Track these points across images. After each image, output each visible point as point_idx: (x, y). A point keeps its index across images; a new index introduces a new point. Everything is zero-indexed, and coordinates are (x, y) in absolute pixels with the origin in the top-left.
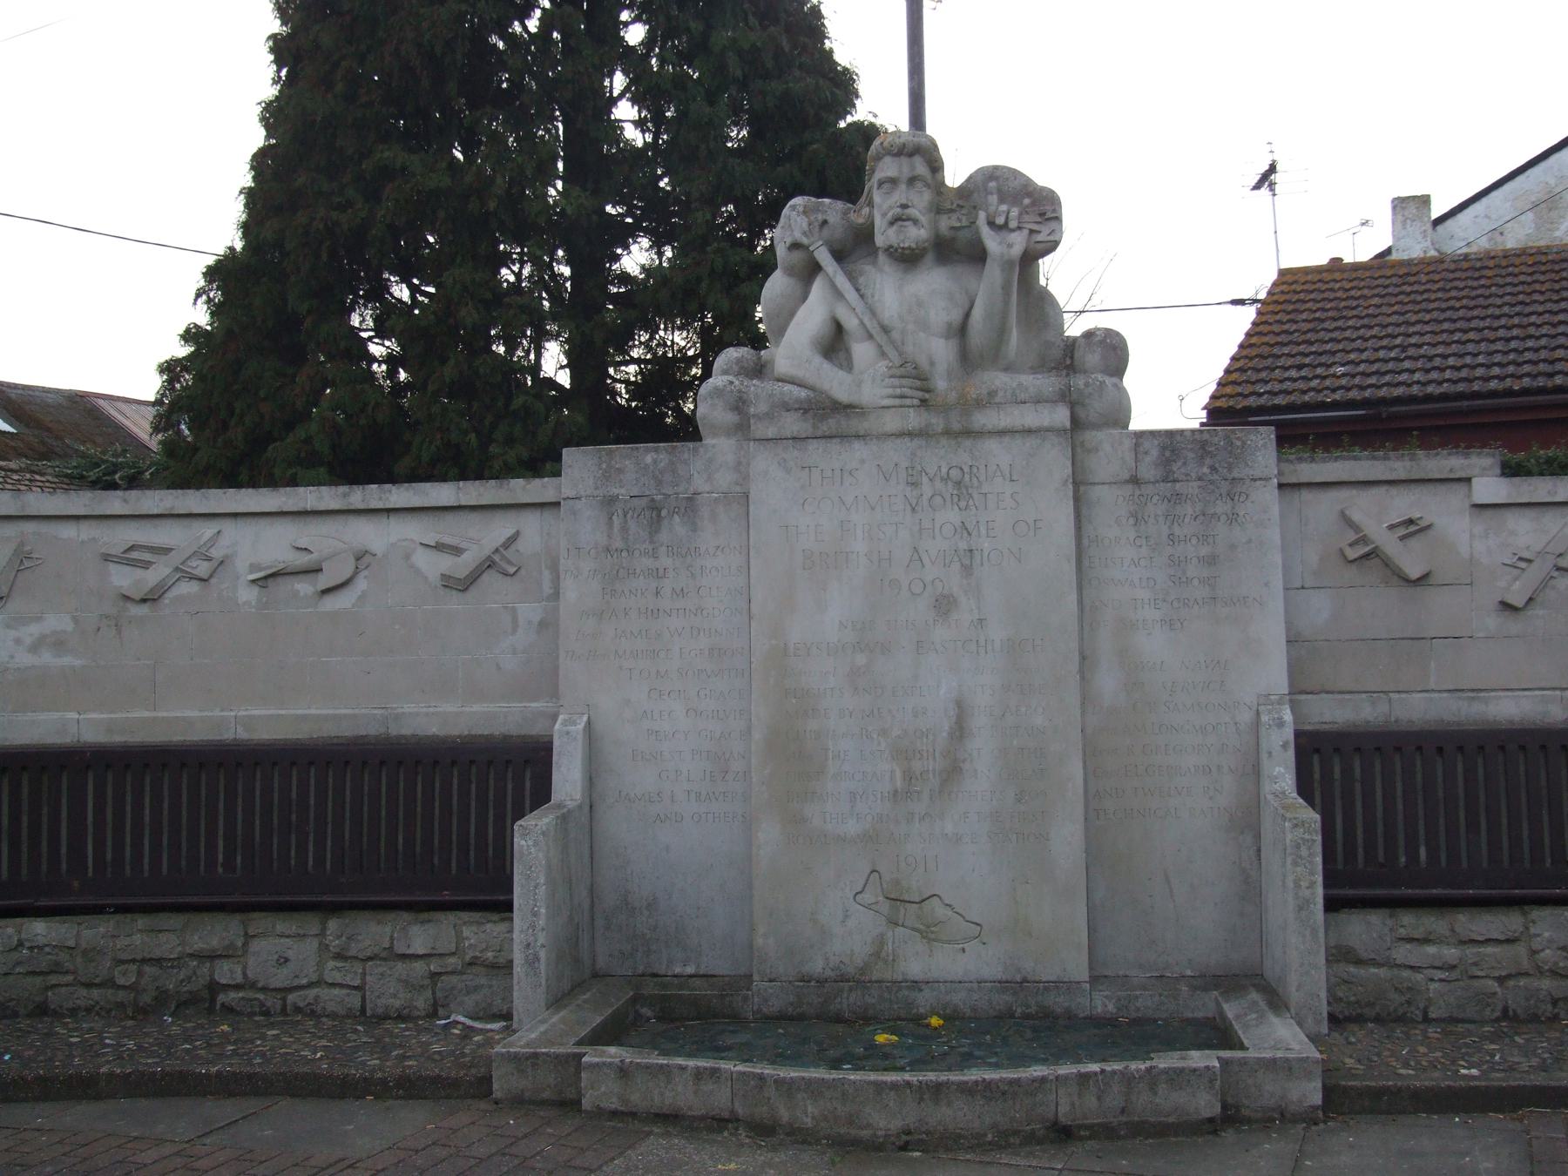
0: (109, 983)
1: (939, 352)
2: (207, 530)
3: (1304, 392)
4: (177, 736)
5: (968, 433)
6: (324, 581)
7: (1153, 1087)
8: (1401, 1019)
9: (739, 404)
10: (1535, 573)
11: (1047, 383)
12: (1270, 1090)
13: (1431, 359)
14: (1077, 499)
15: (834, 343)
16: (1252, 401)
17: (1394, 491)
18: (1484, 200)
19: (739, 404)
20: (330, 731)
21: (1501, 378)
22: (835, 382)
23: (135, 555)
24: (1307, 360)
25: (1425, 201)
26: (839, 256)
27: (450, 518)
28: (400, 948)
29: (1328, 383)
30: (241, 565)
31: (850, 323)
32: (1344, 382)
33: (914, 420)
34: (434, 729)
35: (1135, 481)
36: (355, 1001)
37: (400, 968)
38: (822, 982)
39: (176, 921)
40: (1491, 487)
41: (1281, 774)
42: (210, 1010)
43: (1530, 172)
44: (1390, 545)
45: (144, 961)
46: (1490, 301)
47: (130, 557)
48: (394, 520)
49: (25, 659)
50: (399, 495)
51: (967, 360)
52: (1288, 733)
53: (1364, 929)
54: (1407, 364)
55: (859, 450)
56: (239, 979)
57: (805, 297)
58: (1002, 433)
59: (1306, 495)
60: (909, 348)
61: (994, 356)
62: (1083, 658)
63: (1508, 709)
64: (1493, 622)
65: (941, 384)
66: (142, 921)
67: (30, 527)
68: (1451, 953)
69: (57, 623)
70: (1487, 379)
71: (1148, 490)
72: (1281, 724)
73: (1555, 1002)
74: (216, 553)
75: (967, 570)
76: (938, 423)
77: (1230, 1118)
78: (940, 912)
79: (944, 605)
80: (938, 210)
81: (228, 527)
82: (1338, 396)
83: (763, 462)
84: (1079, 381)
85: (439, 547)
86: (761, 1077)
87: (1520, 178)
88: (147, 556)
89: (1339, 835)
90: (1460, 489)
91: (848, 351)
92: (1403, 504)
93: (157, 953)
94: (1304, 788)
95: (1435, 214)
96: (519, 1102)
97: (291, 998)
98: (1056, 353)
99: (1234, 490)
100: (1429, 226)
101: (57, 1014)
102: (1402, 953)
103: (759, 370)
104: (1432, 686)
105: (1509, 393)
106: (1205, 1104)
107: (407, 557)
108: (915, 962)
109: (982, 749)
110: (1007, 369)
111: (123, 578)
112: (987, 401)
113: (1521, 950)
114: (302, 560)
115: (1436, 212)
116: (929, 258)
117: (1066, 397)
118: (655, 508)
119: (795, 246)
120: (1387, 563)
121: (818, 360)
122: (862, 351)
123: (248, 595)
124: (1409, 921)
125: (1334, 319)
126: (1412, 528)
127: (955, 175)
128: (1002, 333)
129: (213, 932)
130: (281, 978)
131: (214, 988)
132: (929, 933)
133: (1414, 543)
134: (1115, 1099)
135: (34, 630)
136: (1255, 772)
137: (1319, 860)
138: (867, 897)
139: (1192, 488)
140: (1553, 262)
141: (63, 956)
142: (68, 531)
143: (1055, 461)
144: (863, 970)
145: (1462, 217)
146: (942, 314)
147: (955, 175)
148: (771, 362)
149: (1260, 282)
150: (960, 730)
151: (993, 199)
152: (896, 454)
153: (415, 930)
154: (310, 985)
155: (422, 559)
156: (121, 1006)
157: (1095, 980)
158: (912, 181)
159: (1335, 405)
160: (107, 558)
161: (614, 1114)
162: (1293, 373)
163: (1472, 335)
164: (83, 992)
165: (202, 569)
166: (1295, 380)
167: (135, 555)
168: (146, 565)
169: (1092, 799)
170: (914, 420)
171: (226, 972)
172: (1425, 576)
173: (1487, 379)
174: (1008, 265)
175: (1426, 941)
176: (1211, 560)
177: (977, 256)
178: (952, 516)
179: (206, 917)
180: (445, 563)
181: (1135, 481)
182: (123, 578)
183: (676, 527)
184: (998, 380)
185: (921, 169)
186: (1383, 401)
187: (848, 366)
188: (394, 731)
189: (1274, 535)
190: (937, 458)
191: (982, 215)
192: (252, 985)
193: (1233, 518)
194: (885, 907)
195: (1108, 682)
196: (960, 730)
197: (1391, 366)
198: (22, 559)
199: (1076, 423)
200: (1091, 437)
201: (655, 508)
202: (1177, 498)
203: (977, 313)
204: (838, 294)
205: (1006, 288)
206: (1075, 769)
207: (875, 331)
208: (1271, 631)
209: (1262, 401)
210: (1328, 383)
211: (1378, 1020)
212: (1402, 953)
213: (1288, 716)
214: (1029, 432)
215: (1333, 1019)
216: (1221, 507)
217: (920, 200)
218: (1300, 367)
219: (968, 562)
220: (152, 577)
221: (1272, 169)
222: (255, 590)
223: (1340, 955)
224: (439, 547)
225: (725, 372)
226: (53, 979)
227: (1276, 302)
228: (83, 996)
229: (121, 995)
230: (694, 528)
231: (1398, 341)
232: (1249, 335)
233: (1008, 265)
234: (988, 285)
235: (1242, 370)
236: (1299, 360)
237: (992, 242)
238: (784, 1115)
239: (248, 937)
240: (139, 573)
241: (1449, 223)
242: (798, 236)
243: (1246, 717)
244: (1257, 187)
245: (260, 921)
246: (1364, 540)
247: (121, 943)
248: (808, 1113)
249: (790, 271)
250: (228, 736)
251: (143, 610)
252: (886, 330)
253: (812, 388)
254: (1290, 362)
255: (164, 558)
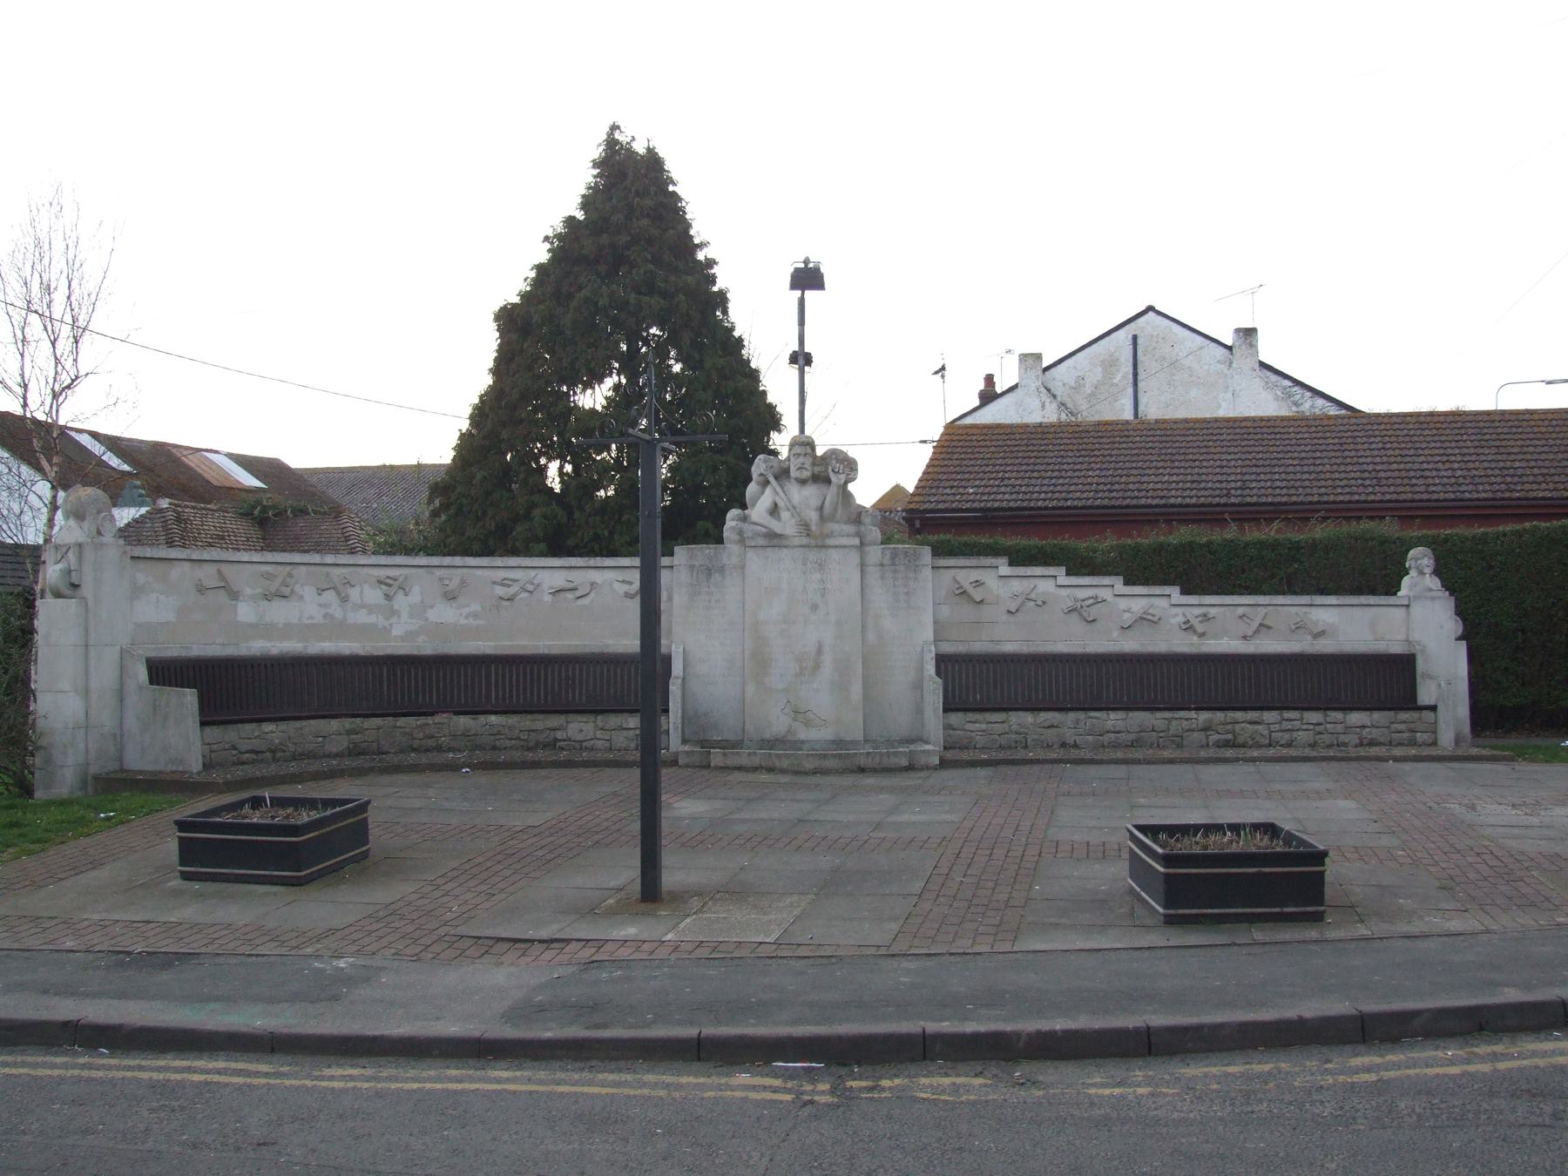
0: (518, 738)
1: (813, 516)
2: (532, 573)
3: (953, 502)
4: (521, 652)
5: (824, 547)
6: (578, 593)
7: (888, 757)
8: (967, 748)
9: (741, 533)
10: (1019, 600)
11: (851, 529)
12: (923, 760)
13: (1014, 487)
14: (862, 571)
15: (774, 511)
16: (927, 506)
17: (972, 570)
18: (1074, 358)
19: (741, 533)
20: (580, 650)
21: (1044, 500)
22: (776, 526)
23: (505, 582)
24: (956, 484)
25: (1038, 357)
26: (776, 478)
27: (627, 570)
28: (625, 726)
29: (964, 498)
30: (545, 587)
31: (781, 504)
32: (972, 497)
33: (805, 541)
34: (621, 650)
35: (882, 565)
36: (608, 745)
37: (625, 733)
38: (769, 741)
39: (541, 716)
40: (1005, 570)
41: (930, 669)
42: (554, 748)
43: (1101, 342)
44: (970, 589)
45: (530, 731)
46: (1047, 454)
47: (504, 583)
48: (606, 570)
49: (463, 622)
50: (609, 562)
51: (823, 519)
52: (933, 655)
53: (956, 718)
54: (1002, 489)
55: (785, 551)
56: (565, 737)
57: (763, 493)
58: (836, 547)
59: (942, 571)
60: (803, 515)
61: (832, 518)
62: (863, 627)
63: (1009, 648)
64: (1004, 617)
65: (814, 528)
66: (529, 716)
67: (465, 570)
68: (984, 726)
69: (475, 607)
70: (1038, 500)
71: (886, 568)
72: (930, 651)
73: (1016, 742)
74: (535, 582)
75: (823, 595)
76: (813, 542)
77: (910, 768)
78: (811, 716)
79: (815, 607)
80: (814, 464)
81: (541, 571)
82: (968, 505)
83: (751, 554)
84: (863, 528)
85: (623, 582)
86: (770, 754)
87: (1094, 346)
88: (510, 583)
89: (957, 693)
90: (995, 570)
91: (779, 513)
92: (975, 575)
93: (535, 728)
94: (938, 673)
95: (1044, 366)
96: (687, 766)
97: (585, 744)
98: (854, 516)
99: (917, 569)
100: (1040, 372)
101: (499, 749)
102: (969, 726)
103: (744, 519)
104: (984, 638)
105: (1046, 508)
106: (904, 762)
107: (611, 585)
108: (803, 734)
109: (827, 659)
110: (837, 522)
111: (500, 591)
112: (831, 535)
113: (1006, 725)
114: (570, 585)
115: (1046, 363)
116: (810, 481)
117: (858, 534)
118: (709, 570)
119: (761, 475)
120: (969, 596)
121: (769, 517)
122: (785, 515)
123: (548, 598)
124: (971, 716)
125: (971, 459)
126: (978, 584)
127: (820, 452)
128: (836, 509)
129: (555, 721)
130: (580, 737)
131: (556, 740)
132: (807, 724)
133: (978, 589)
134: (877, 759)
135: (466, 611)
136: (921, 668)
137: (941, 695)
138: (786, 711)
139: (902, 568)
140: (1082, 432)
141: (501, 729)
142: (479, 572)
143: (854, 558)
144: (785, 736)
145: (1060, 367)
146: (815, 502)
147: (820, 452)
148: (749, 516)
149: (936, 432)
150: (820, 651)
151: (834, 462)
152: (798, 553)
153: (630, 719)
154: (592, 739)
155: (616, 586)
156: (523, 746)
157: (866, 741)
158: (805, 455)
159: (967, 510)
160: (494, 583)
161: (721, 768)
162: (948, 491)
163: (1035, 474)
164: (508, 742)
165: (530, 588)
166: (948, 495)
167: (505, 582)
168: (509, 586)
169: (865, 678)
170: (805, 541)
171: (559, 735)
172: (982, 601)
173: (1038, 500)
174: (839, 487)
175: (975, 722)
176: (907, 594)
177: (828, 481)
178: (817, 576)
179: (551, 715)
180: (626, 588)
181: (882, 565)
182: (500, 591)
183: (717, 577)
184: (835, 527)
185: (809, 450)
186: (989, 509)
187: (779, 519)
188: (605, 651)
189: (930, 585)
190: (813, 555)
191: (830, 470)
192: (570, 740)
193: (916, 579)
194: (792, 715)
195: (871, 636)
196: (820, 651)
197: (995, 489)
198: (463, 583)
199: (862, 544)
200: (868, 549)
201: (709, 570)
202: (895, 571)
203: (827, 502)
204: (777, 493)
205: (838, 494)
206: (860, 666)
207: (791, 508)
208: (928, 619)
209: (932, 506)
210: (964, 498)
211: (959, 748)
212: (969, 726)
213: (933, 648)
214: (845, 547)
215: (945, 748)
216: (912, 575)
217: (808, 461)
218: (952, 487)
219: (823, 593)
220: (512, 590)
221: (943, 368)
222: (551, 596)
223: (948, 727)
224: (623, 582)
225: (733, 520)
226: (498, 737)
227: (943, 447)
228: (508, 743)
229: (522, 743)
230: (724, 577)
231: (1000, 475)
232: (928, 466)
233: (839, 487)
234: (831, 493)
235: (923, 487)
236: (951, 483)
237: (833, 478)
238: (778, 765)
239: (567, 722)
240: (505, 589)
241: (1053, 370)
242: (763, 472)
243: (918, 649)
244: (936, 373)
245: (572, 717)
246: (961, 587)
247: (522, 724)
248: (785, 764)
249: (758, 483)
250: (541, 652)
251: (507, 603)
252: (794, 508)
253: (766, 527)
254: (948, 484)
255: (516, 583)
